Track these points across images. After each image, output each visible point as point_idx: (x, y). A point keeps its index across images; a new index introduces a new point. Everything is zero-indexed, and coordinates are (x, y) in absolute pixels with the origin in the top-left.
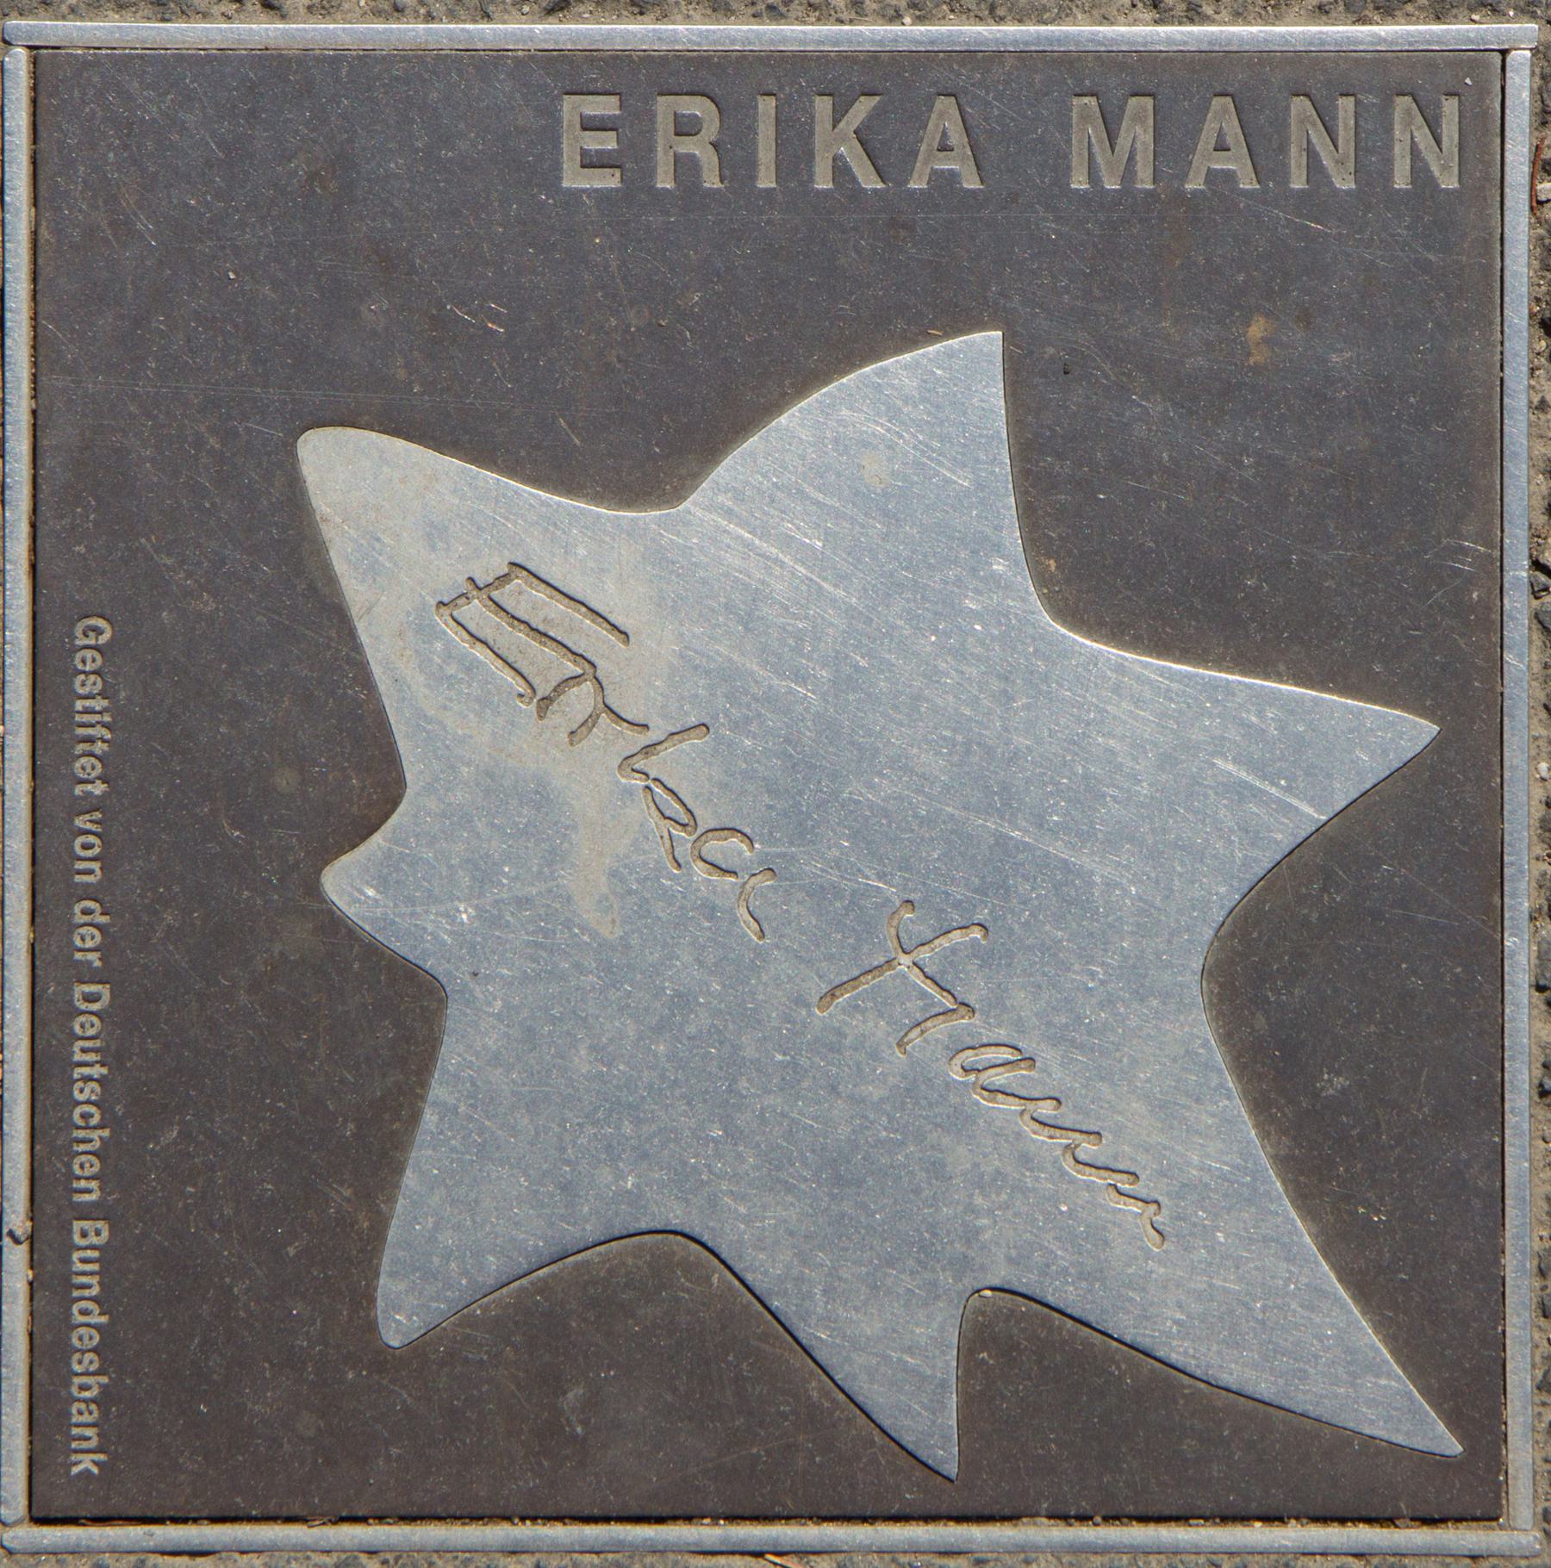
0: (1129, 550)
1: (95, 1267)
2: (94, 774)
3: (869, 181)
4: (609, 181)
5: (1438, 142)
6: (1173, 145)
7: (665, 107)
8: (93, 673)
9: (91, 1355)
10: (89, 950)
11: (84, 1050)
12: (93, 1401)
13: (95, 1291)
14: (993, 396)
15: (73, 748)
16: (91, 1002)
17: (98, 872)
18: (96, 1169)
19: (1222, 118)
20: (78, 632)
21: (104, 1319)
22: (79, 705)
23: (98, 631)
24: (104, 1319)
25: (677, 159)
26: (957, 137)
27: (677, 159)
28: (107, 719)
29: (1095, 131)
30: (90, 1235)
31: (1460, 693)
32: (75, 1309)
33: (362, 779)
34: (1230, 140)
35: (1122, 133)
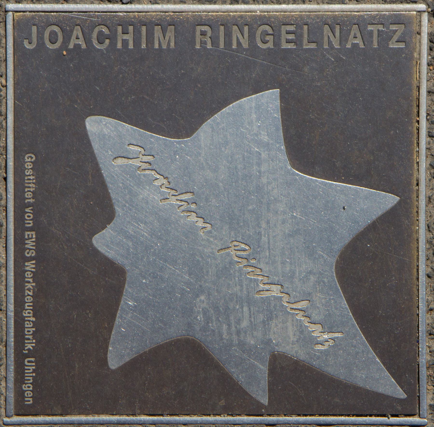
0: (311, 146)
1: (31, 308)
5: (164, 38)
6: (343, 39)
9: (31, 170)
13: (31, 381)
14: (278, 95)
15: (25, 200)
16: (30, 366)
18: (31, 276)
19: (77, 32)
20: (26, 158)
22: (26, 178)
23: (32, 158)
26: (358, 35)
28: (34, 181)
30: (30, 266)
31: (400, 183)
33: (100, 208)
35: (166, 36)
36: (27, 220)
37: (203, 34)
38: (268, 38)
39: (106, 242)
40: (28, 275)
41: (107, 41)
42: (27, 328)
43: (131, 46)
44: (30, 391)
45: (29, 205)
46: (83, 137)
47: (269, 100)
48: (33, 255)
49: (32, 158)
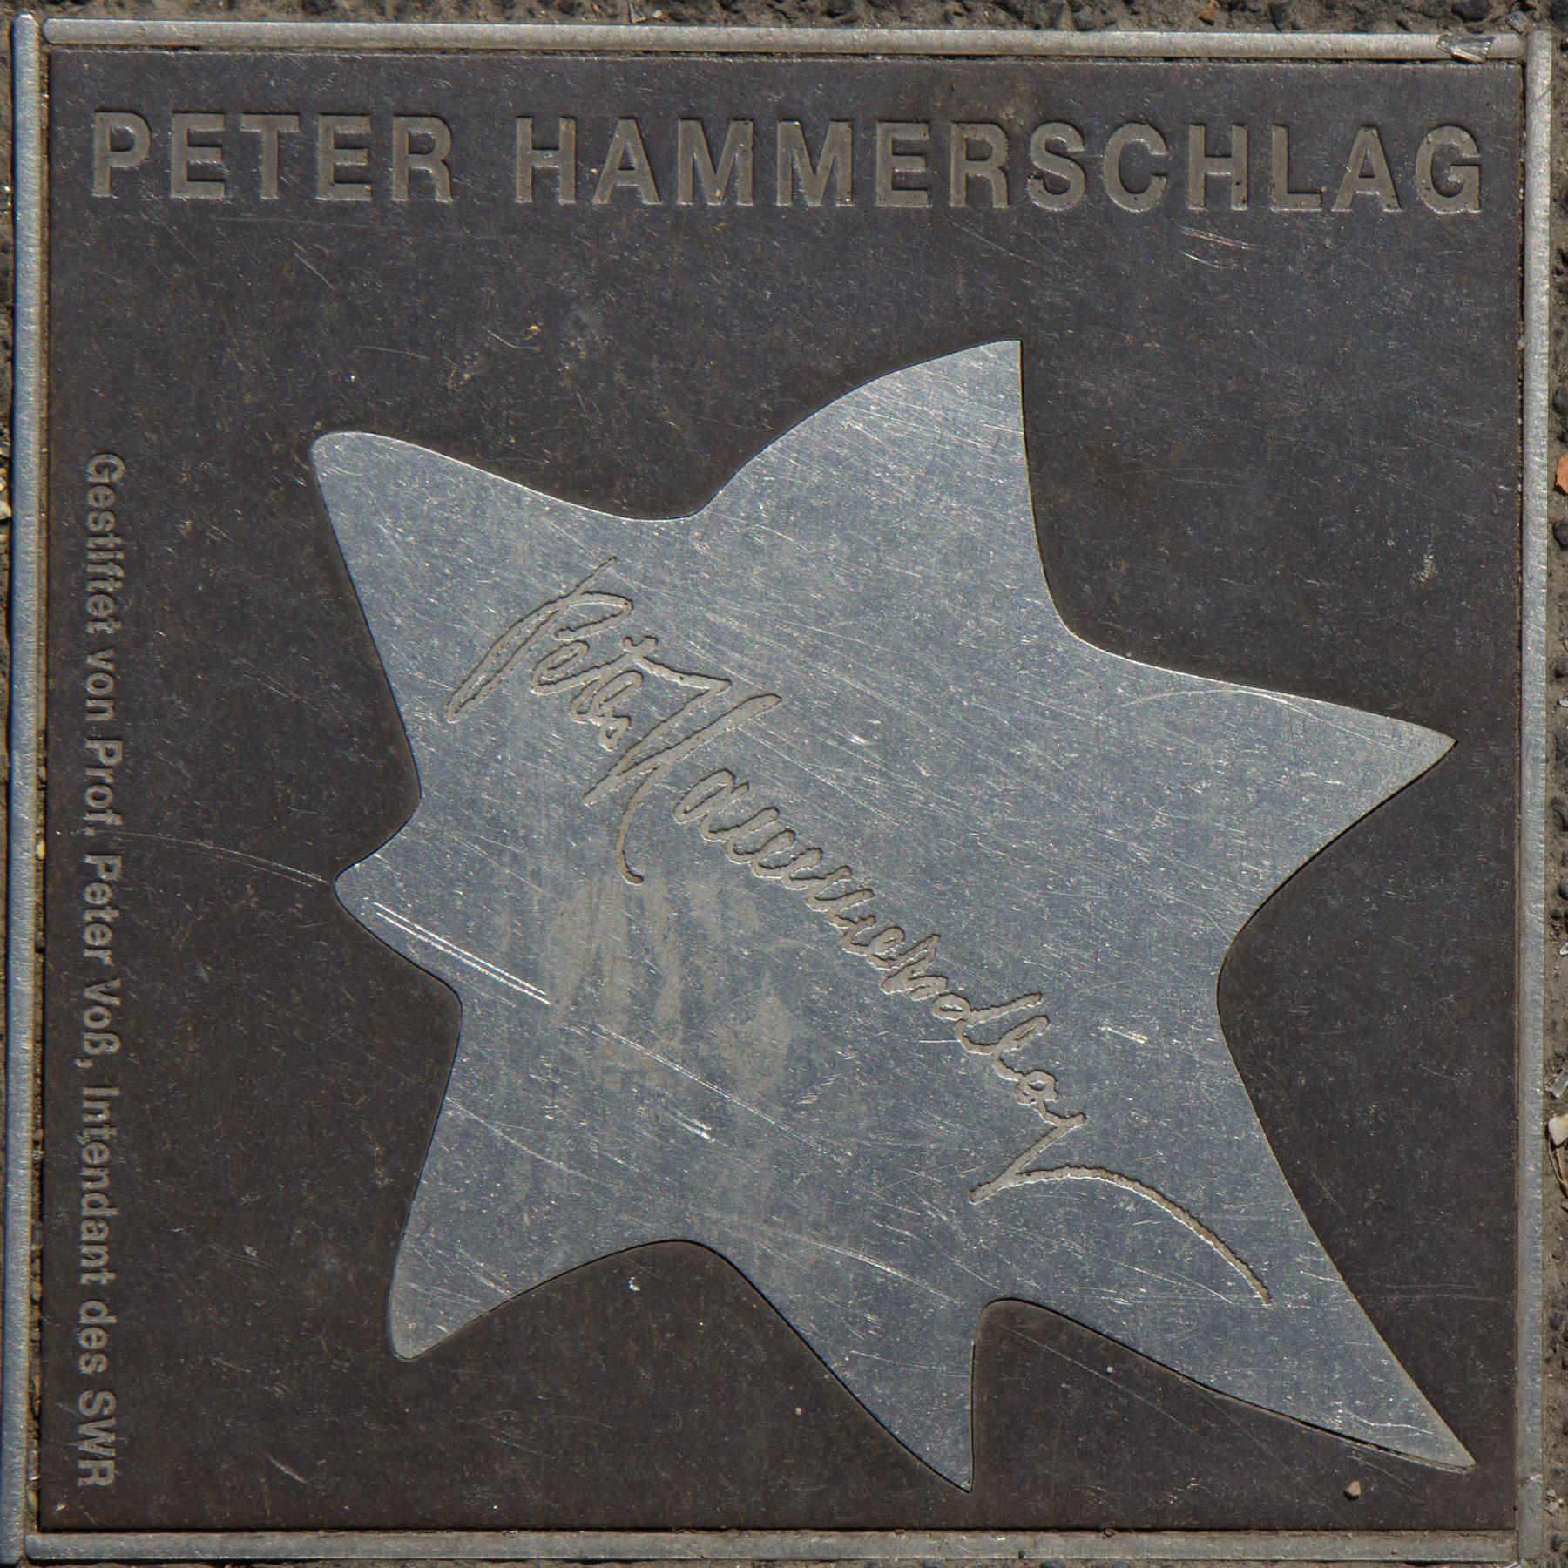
0: (1135, 544)
2: (105, 901)
4: (215, 193)
7: (401, 130)
10: (101, 908)
13: (104, 1184)
15: (82, 913)
17: (106, 1257)
19: (625, 139)
21: (112, 1320)
23: (113, 469)
24: (112, 1320)
25: (970, 183)
27: (970, 183)
28: (120, 556)
29: (700, 157)
31: (1474, 706)
32: (84, 1202)
33: (372, 785)
34: (634, 162)
36: (91, 698)
37: (420, 147)
38: (1453, 178)
39: (382, 897)
40: (89, 1339)
41: (1158, 185)
43: (81, 1482)
44: (110, 486)
45: (100, 644)
48: (87, 1395)
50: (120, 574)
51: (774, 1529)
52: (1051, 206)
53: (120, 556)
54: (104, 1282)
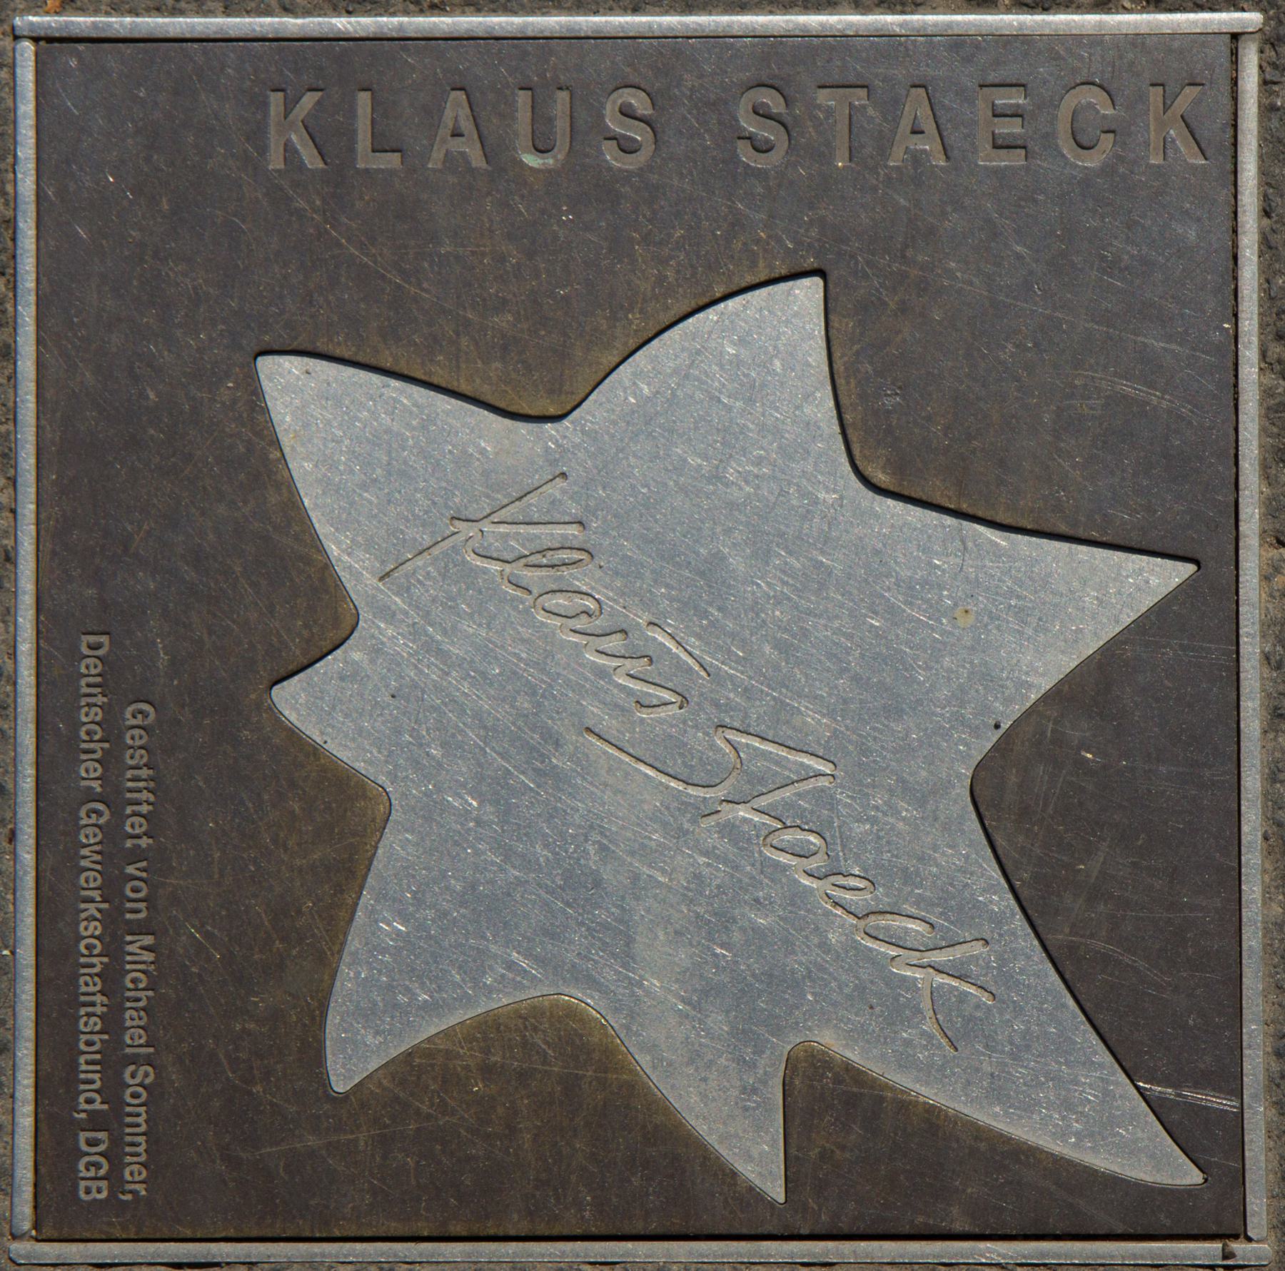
0: (920, 434)
3: (83, 915)
8: (141, 747)
11: (88, 685)
12: (97, 975)
13: (97, 1085)
15: (124, 809)
23: (145, 715)
26: (467, 125)
32: (82, 1099)
34: (924, 127)
36: (129, 1105)
42: (83, 1179)
44: (100, 1154)
45: (135, 856)
46: (254, 456)
47: (787, 322)
48: (132, 1067)
49: (99, 814)
50: (152, 798)
51: (37, 133)
52: (759, 162)
53: (152, 784)
54: (144, 846)
